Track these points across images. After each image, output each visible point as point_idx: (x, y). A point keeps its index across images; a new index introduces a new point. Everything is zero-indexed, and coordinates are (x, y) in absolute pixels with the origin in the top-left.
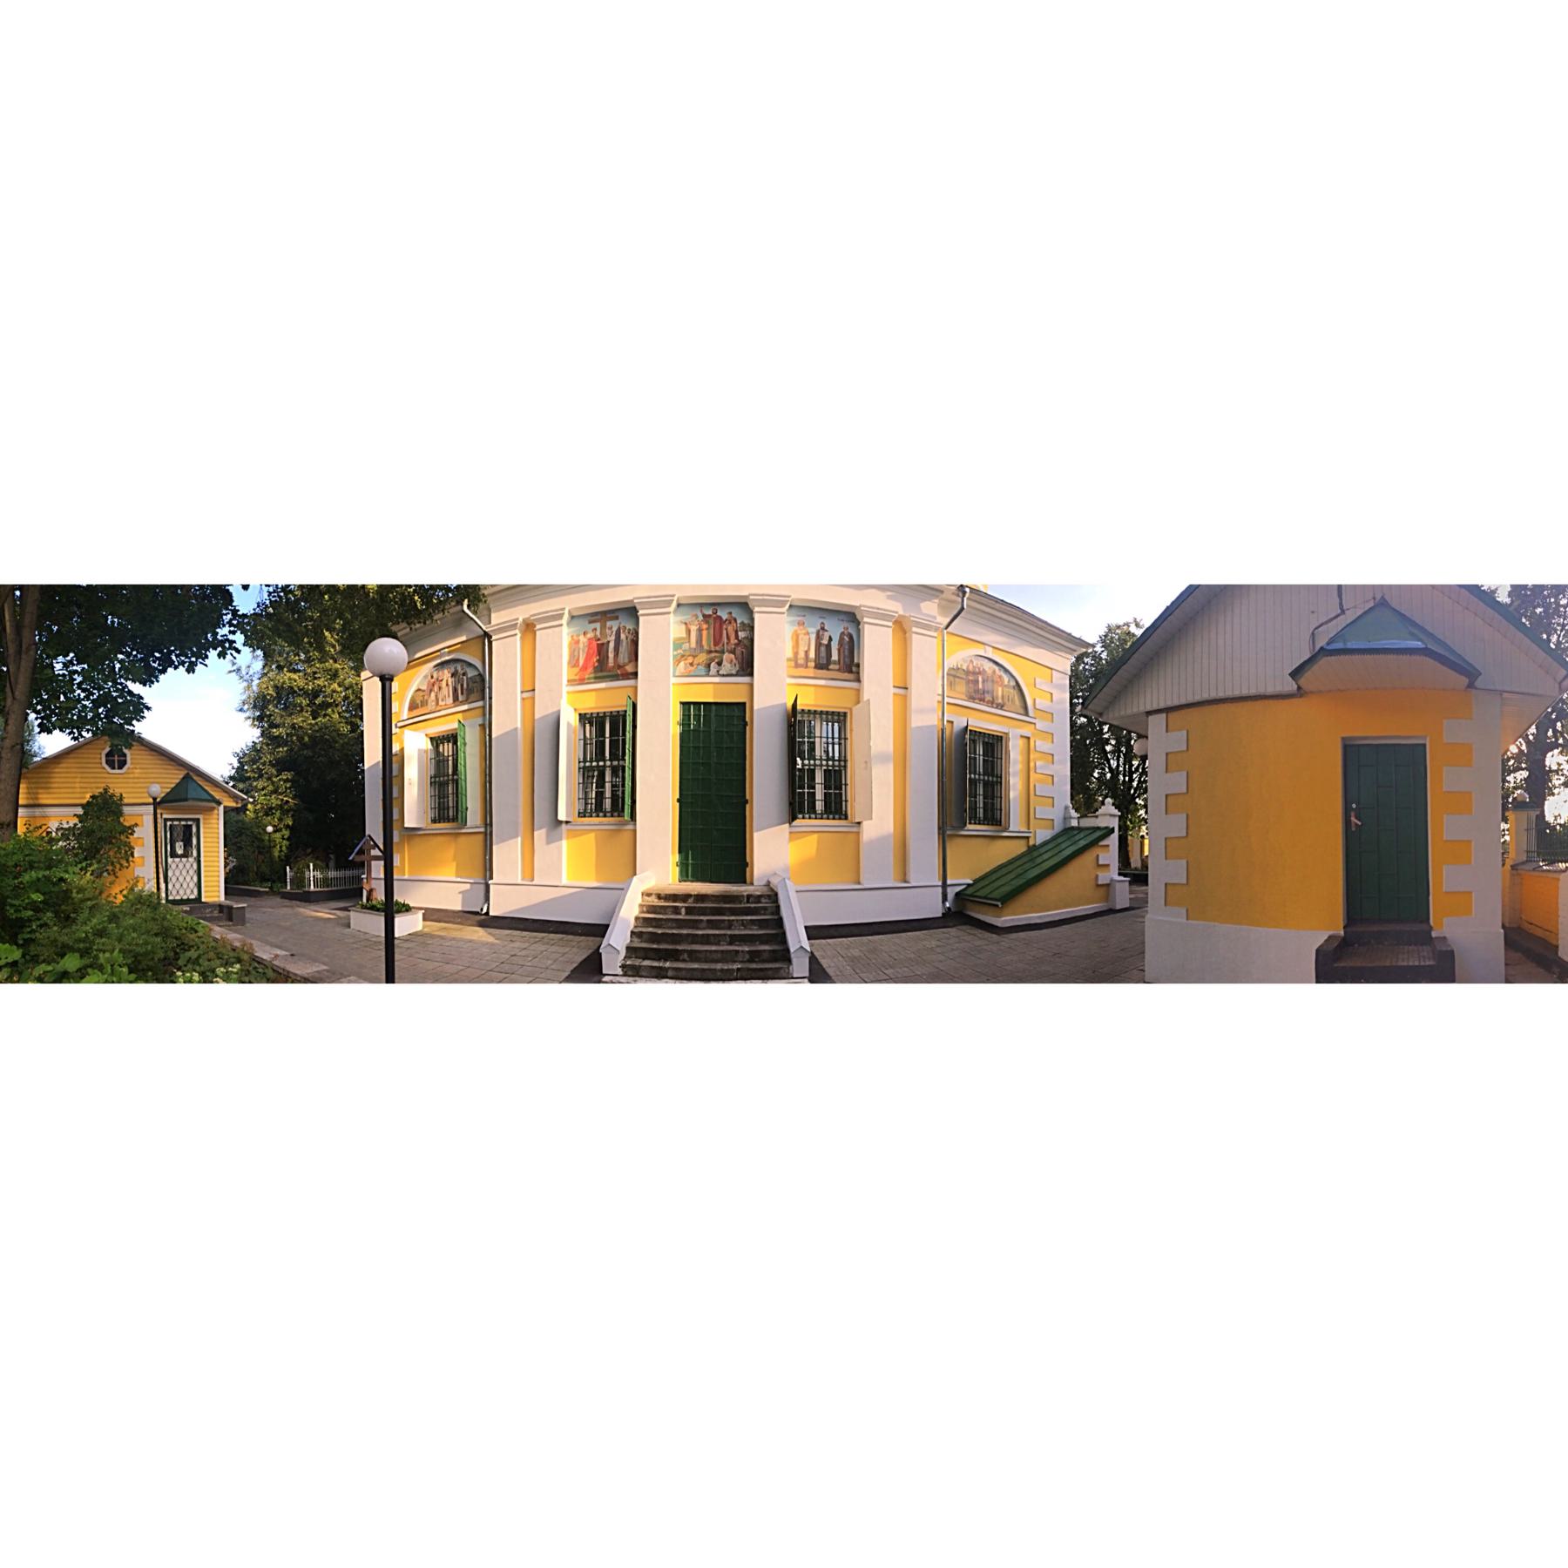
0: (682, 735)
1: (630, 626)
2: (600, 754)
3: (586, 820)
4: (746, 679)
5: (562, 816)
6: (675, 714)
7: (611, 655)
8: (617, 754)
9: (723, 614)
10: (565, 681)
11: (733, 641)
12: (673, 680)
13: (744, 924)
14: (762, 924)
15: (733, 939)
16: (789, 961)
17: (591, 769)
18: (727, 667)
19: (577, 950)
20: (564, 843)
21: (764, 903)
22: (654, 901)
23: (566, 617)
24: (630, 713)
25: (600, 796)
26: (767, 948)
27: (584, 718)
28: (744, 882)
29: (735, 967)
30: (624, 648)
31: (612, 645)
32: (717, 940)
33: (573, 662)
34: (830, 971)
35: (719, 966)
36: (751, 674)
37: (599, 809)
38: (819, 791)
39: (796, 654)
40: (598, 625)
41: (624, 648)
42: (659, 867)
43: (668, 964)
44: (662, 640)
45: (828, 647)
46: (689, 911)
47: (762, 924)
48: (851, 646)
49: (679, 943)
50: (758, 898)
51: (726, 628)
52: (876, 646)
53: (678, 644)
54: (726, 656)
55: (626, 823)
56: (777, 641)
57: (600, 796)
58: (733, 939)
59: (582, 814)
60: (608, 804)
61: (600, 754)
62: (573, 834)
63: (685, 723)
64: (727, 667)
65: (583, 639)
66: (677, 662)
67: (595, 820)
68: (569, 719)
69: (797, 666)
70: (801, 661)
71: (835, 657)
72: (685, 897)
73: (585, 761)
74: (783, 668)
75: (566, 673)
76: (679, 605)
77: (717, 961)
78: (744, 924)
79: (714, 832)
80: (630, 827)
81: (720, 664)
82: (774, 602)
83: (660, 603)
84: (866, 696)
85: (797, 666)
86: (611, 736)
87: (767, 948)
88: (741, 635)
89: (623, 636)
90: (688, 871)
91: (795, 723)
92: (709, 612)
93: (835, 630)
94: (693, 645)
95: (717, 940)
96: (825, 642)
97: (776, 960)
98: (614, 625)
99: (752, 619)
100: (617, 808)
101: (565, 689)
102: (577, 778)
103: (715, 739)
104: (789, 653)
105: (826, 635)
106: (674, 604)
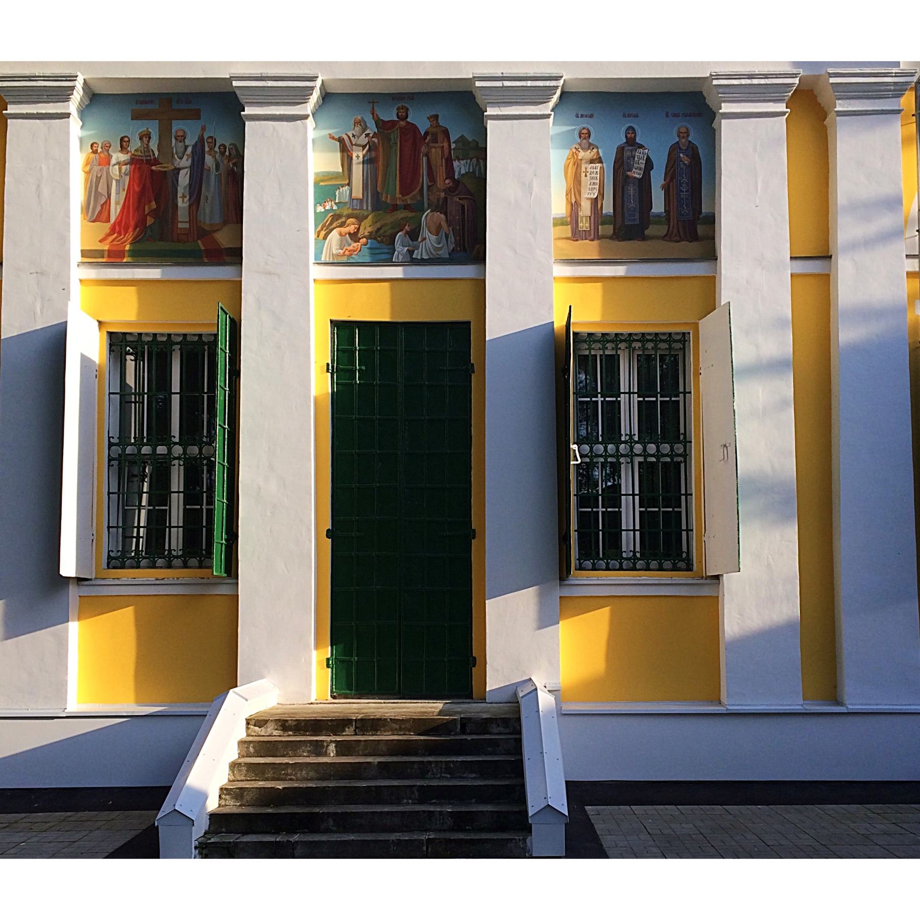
0: (336, 398)
1: (224, 138)
2: (158, 428)
3: (127, 574)
4: (466, 271)
5: (68, 567)
6: (319, 349)
7: (182, 204)
8: (196, 426)
9: (420, 120)
10: (75, 256)
11: (443, 182)
12: (317, 272)
13: (449, 769)
14: (482, 769)
15: (426, 794)
16: (528, 829)
17: (138, 460)
18: (429, 241)
19: (130, 823)
20: (74, 628)
21: (496, 734)
22: (272, 733)
23: (77, 95)
24: (223, 345)
25: (158, 522)
26: (489, 808)
27: (119, 343)
28: (469, 696)
29: (424, 837)
30: (211, 190)
31: (184, 179)
32: (395, 795)
33: (96, 211)
34: (606, 841)
35: (394, 837)
36: (480, 258)
37: (155, 551)
38: (631, 500)
39: (574, 207)
40: (153, 127)
41: (211, 190)
42: (286, 667)
43: (296, 838)
44: (293, 172)
45: (644, 184)
46: (344, 748)
47: (482, 769)
48: (694, 174)
49: (319, 804)
50: (484, 725)
51: (420, 152)
52: (752, 171)
53: (326, 188)
54: (427, 217)
55: (218, 581)
56: (534, 182)
57: (158, 522)
58: (426, 794)
59: (118, 560)
60: (175, 539)
61: (158, 428)
62: (95, 606)
63: (341, 367)
64: (429, 241)
65: (118, 156)
66: (324, 230)
67: (145, 575)
68: (86, 345)
69: (577, 235)
70: (584, 225)
71: (658, 206)
72: (337, 725)
73: (123, 438)
74: (550, 241)
75: (78, 233)
76: (327, 97)
77: (392, 830)
78: (449, 769)
79: (401, 594)
80: (224, 590)
81: (414, 235)
82: (525, 90)
83: (286, 90)
84: (726, 294)
85: (577, 235)
86: (179, 393)
87: (489, 808)
88: (461, 167)
89: (209, 160)
90: (351, 677)
91: (568, 358)
92: (389, 115)
93: (656, 146)
94: (358, 192)
95: (395, 795)
96: (637, 174)
97: (503, 829)
98: (190, 131)
99: (483, 132)
100: (197, 548)
101: (78, 273)
102: (103, 480)
103: (404, 396)
104: (559, 207)
105: (640, 157)
106: (315, 96)
